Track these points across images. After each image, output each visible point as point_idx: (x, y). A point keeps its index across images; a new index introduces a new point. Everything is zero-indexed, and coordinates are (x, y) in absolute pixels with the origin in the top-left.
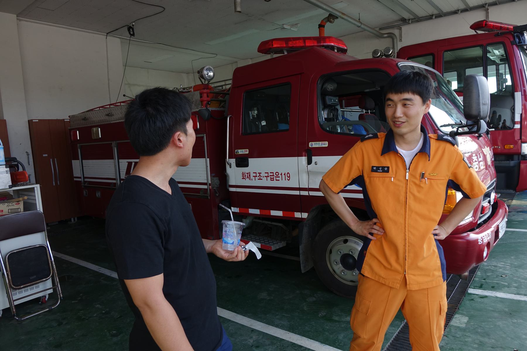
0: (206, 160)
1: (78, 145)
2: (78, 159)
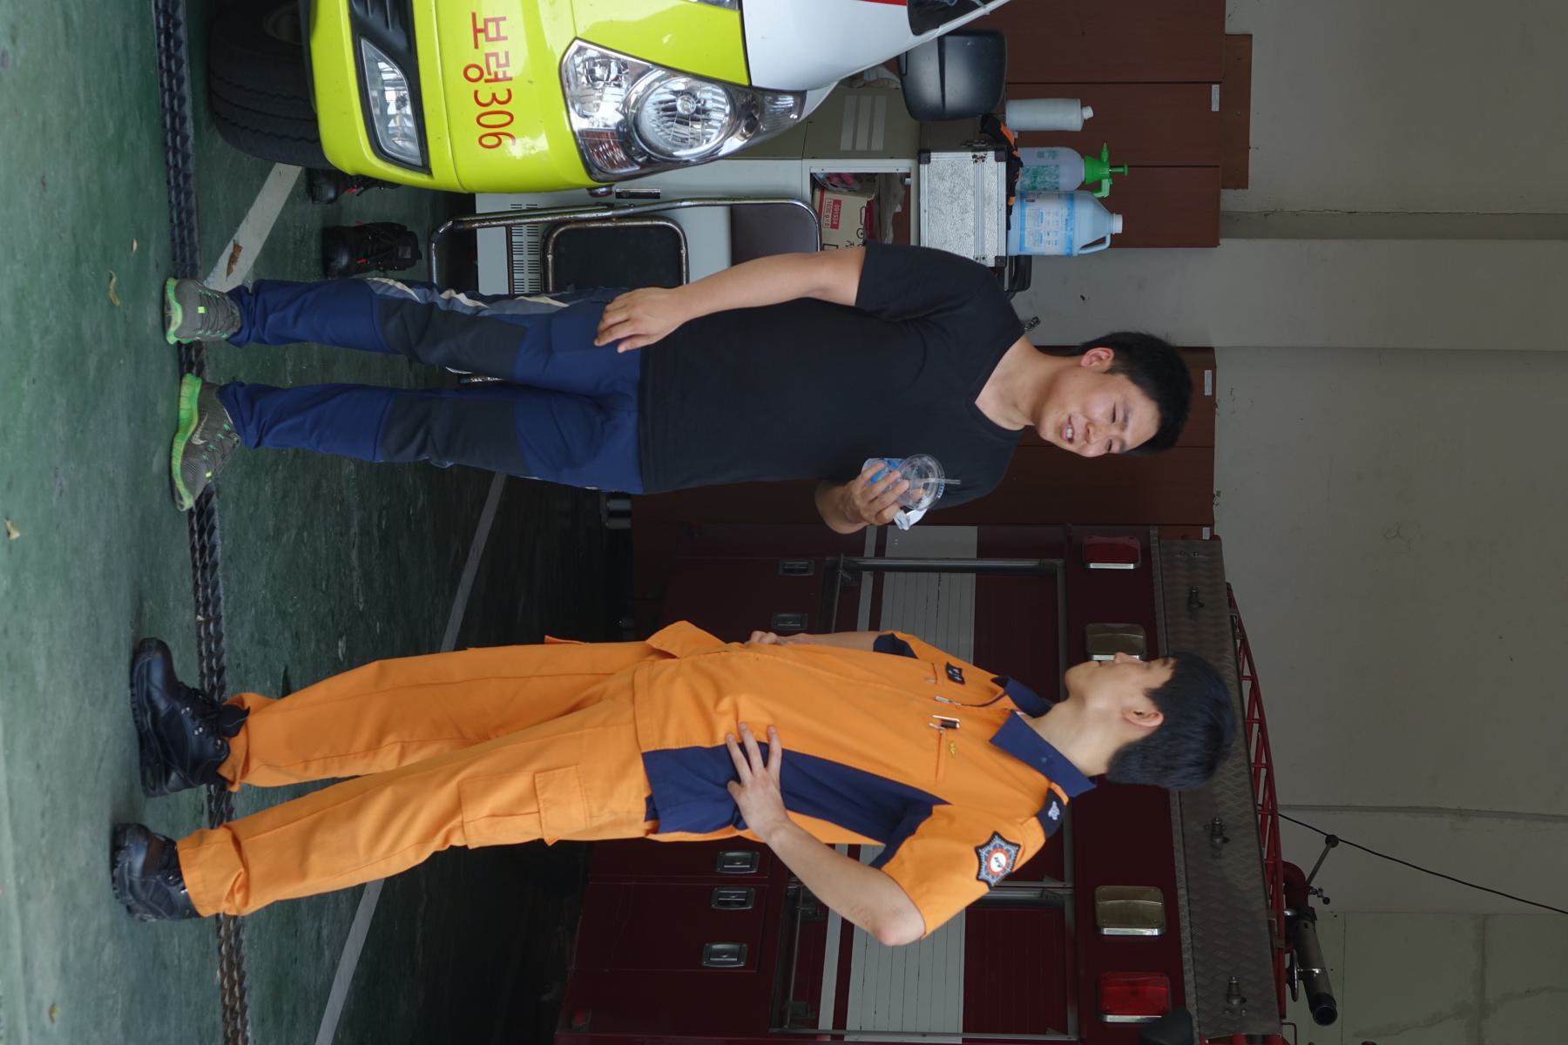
0: (957, 1034)
1: (1059, 562)
2: (982, 554)
